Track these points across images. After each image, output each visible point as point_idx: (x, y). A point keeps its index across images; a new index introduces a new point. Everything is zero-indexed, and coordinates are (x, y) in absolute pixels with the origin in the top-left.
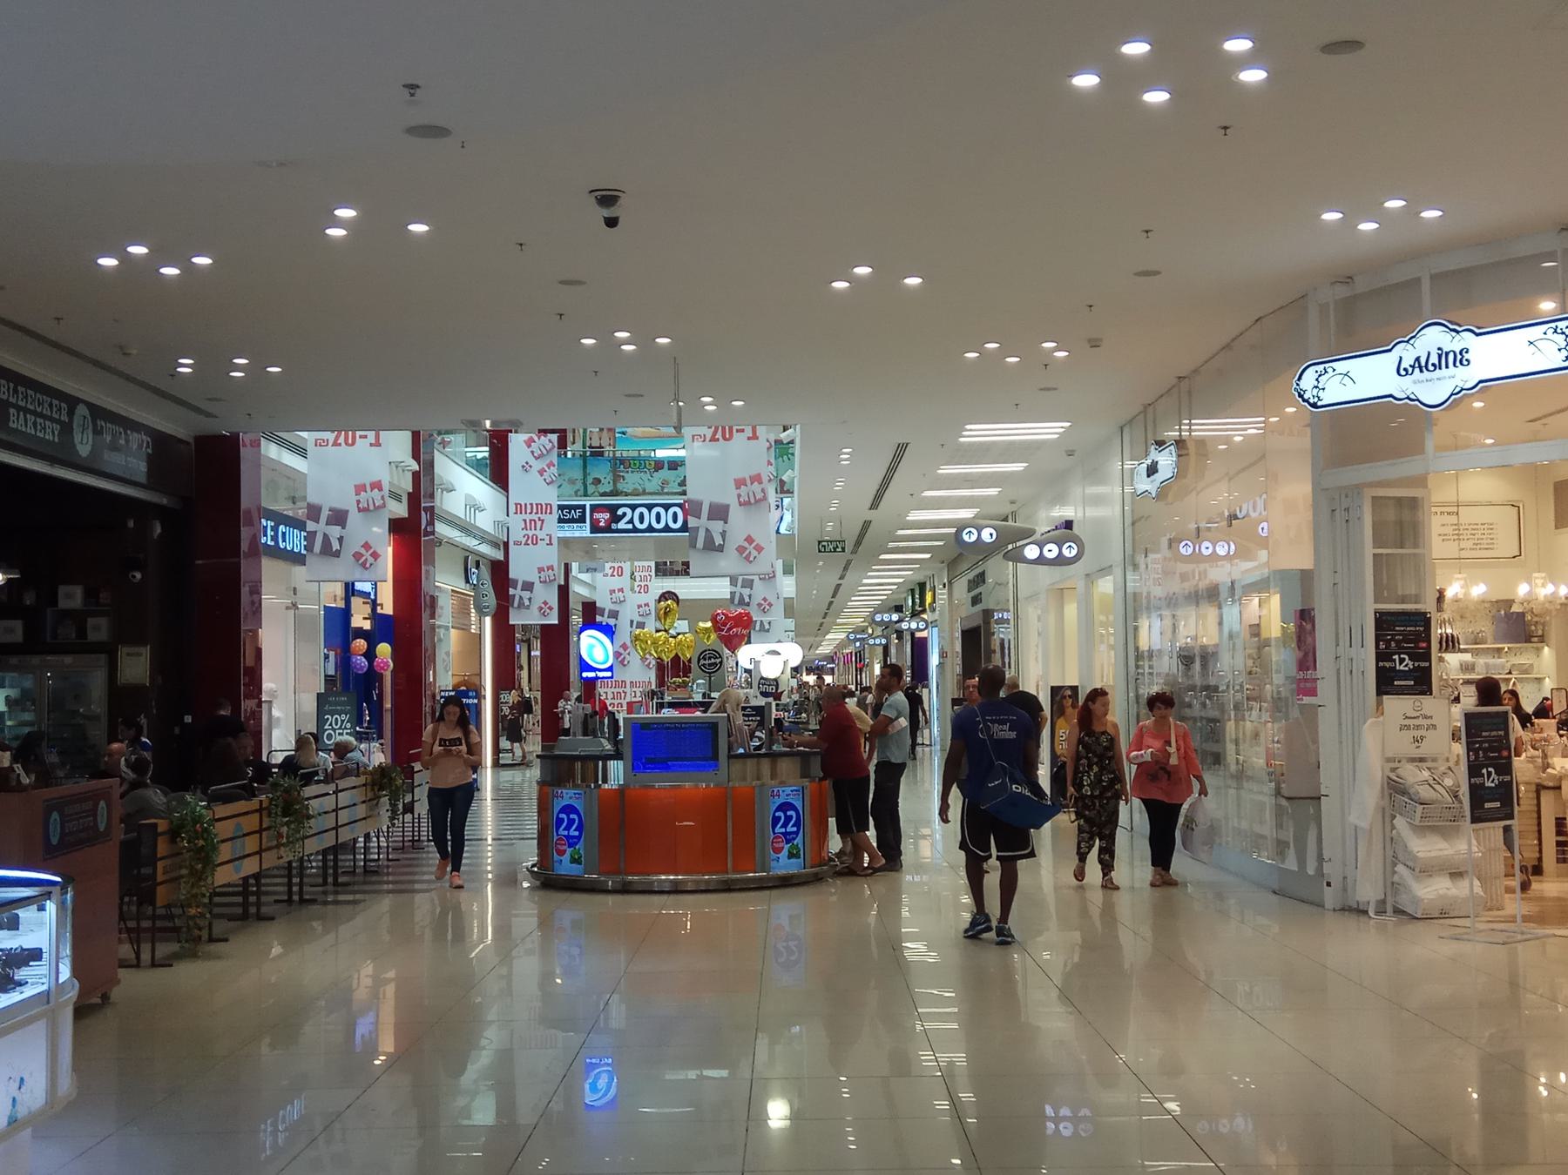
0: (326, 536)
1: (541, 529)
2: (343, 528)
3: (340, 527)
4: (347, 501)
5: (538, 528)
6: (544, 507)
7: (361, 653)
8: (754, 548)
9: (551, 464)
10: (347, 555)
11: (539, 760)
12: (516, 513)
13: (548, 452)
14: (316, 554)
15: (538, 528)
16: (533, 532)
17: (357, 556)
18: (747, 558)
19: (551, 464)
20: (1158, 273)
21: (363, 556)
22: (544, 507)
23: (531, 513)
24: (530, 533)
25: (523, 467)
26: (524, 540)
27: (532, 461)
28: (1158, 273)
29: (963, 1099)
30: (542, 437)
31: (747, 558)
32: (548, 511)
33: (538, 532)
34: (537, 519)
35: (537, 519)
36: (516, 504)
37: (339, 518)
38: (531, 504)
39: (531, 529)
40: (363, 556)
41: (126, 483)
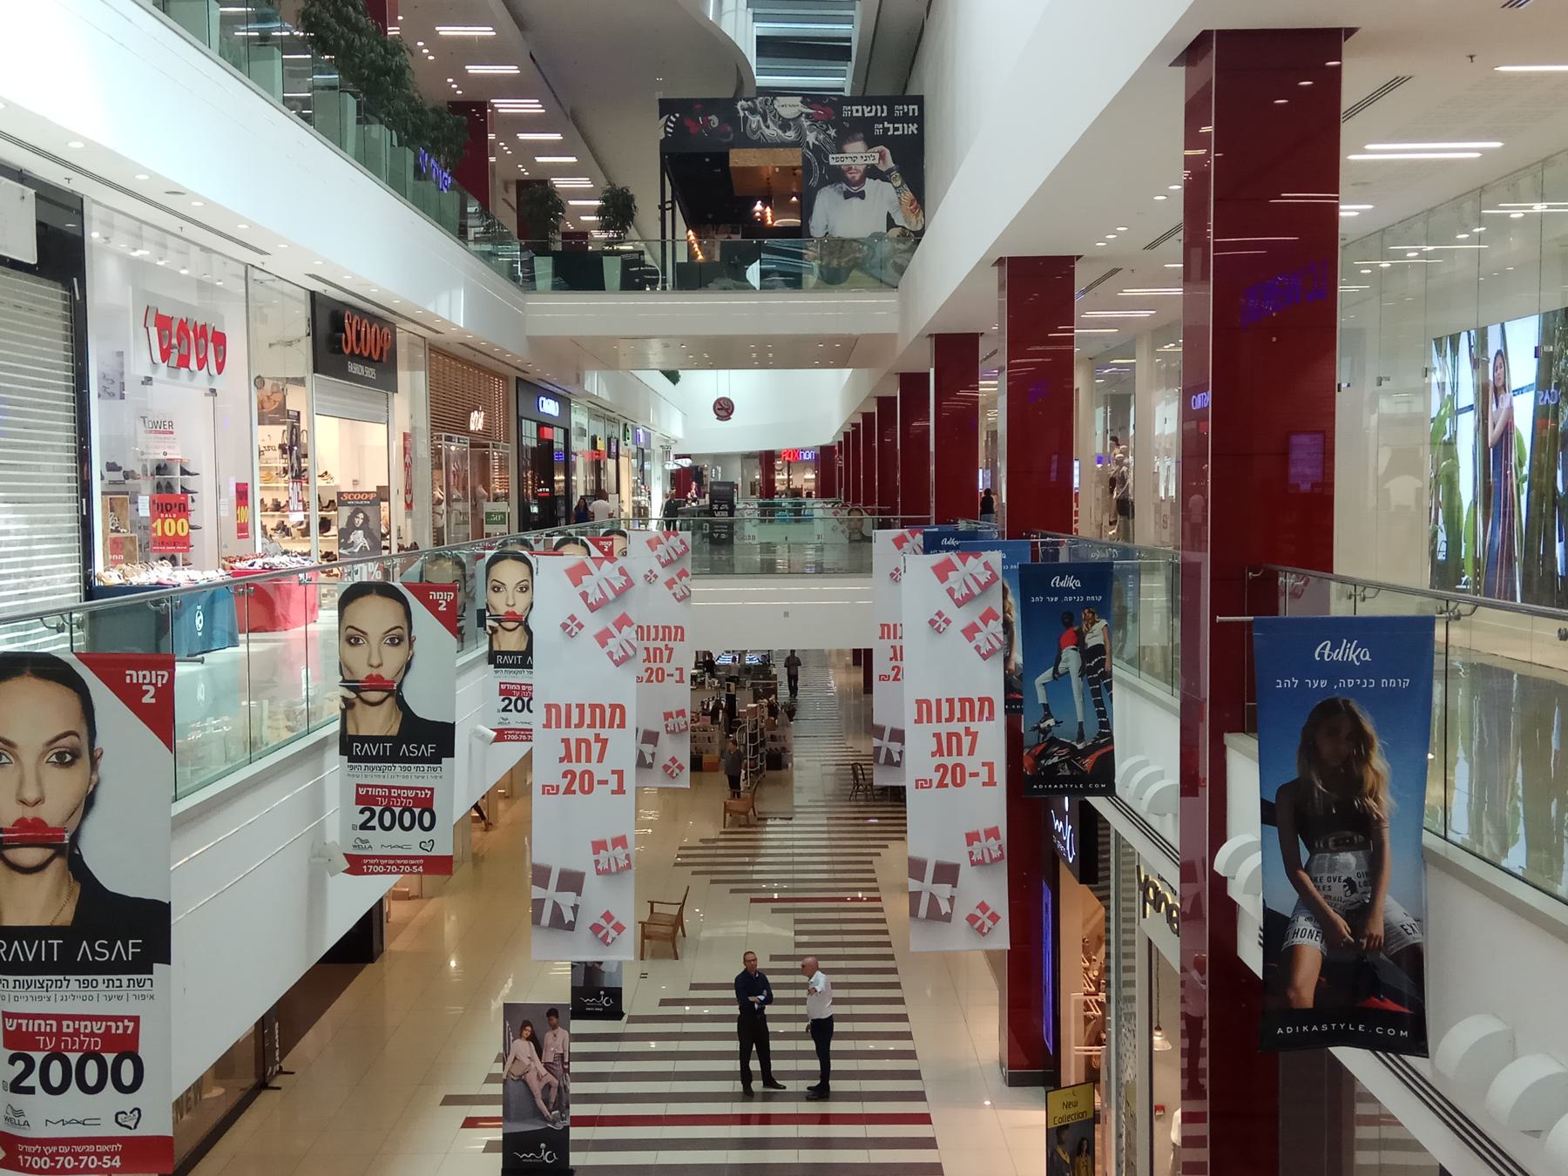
0: (556, 906)
1: (669, 661)
2: (579, 894)
3: (575, 894)
4: (582, 861)
5: (595, 757)
6: (977, 705)
7: (1060, 766)
8: (989, 918)
9: (988, 616)
10: (583, 927)
11: (871, 751)
12: (919, 721)
13: (985, 588)
14: (544, 927)
15: (595, 757)
16: (954, 759)
17: (596, 928)
18: (980, 929)
19: (988, 616)
20: (293, 1073)
21: (603, 928)
22: (977, 705)
23: (950, 720)
24: (949, 761)
25: (932, 622)
26: (936, 777)
27: (582, 613)
28: (293, 1073)
29: (500, 111)
30: (971, 558)
31: (980, 929)
32: (617, 721)
33: (664, 665)
34: (962, 733)
35: (962, 733)
36: (548, 707)
37: (571, 881)
38: (889, 638)
39: (950, 754)
40: (603, 928)
41: (200, 815)
